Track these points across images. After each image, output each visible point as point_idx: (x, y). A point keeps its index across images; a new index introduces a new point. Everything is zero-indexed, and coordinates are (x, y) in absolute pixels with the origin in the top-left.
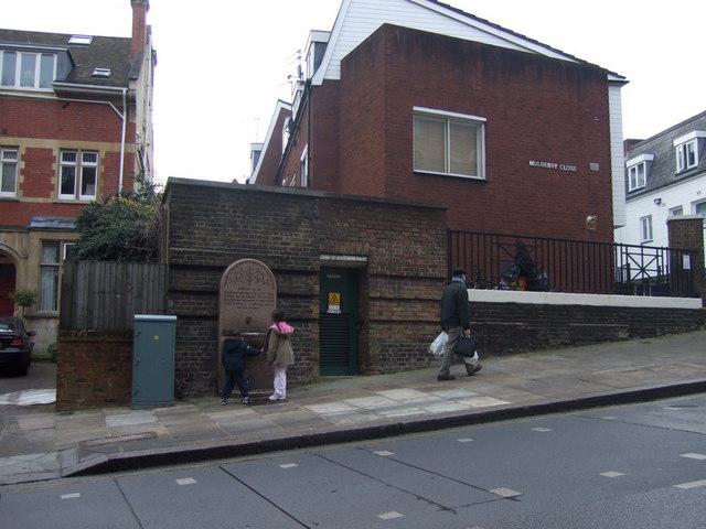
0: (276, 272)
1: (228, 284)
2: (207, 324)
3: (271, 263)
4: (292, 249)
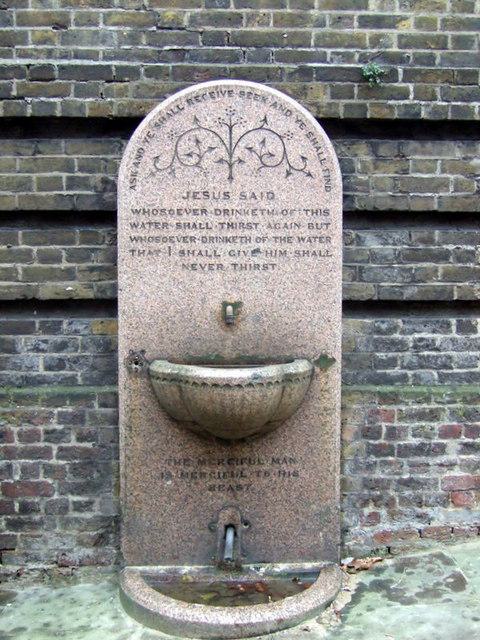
0: (337, 128)
1: (142, 180)
2: (80, 328)
3: (325, 99)
4: (406, 42)
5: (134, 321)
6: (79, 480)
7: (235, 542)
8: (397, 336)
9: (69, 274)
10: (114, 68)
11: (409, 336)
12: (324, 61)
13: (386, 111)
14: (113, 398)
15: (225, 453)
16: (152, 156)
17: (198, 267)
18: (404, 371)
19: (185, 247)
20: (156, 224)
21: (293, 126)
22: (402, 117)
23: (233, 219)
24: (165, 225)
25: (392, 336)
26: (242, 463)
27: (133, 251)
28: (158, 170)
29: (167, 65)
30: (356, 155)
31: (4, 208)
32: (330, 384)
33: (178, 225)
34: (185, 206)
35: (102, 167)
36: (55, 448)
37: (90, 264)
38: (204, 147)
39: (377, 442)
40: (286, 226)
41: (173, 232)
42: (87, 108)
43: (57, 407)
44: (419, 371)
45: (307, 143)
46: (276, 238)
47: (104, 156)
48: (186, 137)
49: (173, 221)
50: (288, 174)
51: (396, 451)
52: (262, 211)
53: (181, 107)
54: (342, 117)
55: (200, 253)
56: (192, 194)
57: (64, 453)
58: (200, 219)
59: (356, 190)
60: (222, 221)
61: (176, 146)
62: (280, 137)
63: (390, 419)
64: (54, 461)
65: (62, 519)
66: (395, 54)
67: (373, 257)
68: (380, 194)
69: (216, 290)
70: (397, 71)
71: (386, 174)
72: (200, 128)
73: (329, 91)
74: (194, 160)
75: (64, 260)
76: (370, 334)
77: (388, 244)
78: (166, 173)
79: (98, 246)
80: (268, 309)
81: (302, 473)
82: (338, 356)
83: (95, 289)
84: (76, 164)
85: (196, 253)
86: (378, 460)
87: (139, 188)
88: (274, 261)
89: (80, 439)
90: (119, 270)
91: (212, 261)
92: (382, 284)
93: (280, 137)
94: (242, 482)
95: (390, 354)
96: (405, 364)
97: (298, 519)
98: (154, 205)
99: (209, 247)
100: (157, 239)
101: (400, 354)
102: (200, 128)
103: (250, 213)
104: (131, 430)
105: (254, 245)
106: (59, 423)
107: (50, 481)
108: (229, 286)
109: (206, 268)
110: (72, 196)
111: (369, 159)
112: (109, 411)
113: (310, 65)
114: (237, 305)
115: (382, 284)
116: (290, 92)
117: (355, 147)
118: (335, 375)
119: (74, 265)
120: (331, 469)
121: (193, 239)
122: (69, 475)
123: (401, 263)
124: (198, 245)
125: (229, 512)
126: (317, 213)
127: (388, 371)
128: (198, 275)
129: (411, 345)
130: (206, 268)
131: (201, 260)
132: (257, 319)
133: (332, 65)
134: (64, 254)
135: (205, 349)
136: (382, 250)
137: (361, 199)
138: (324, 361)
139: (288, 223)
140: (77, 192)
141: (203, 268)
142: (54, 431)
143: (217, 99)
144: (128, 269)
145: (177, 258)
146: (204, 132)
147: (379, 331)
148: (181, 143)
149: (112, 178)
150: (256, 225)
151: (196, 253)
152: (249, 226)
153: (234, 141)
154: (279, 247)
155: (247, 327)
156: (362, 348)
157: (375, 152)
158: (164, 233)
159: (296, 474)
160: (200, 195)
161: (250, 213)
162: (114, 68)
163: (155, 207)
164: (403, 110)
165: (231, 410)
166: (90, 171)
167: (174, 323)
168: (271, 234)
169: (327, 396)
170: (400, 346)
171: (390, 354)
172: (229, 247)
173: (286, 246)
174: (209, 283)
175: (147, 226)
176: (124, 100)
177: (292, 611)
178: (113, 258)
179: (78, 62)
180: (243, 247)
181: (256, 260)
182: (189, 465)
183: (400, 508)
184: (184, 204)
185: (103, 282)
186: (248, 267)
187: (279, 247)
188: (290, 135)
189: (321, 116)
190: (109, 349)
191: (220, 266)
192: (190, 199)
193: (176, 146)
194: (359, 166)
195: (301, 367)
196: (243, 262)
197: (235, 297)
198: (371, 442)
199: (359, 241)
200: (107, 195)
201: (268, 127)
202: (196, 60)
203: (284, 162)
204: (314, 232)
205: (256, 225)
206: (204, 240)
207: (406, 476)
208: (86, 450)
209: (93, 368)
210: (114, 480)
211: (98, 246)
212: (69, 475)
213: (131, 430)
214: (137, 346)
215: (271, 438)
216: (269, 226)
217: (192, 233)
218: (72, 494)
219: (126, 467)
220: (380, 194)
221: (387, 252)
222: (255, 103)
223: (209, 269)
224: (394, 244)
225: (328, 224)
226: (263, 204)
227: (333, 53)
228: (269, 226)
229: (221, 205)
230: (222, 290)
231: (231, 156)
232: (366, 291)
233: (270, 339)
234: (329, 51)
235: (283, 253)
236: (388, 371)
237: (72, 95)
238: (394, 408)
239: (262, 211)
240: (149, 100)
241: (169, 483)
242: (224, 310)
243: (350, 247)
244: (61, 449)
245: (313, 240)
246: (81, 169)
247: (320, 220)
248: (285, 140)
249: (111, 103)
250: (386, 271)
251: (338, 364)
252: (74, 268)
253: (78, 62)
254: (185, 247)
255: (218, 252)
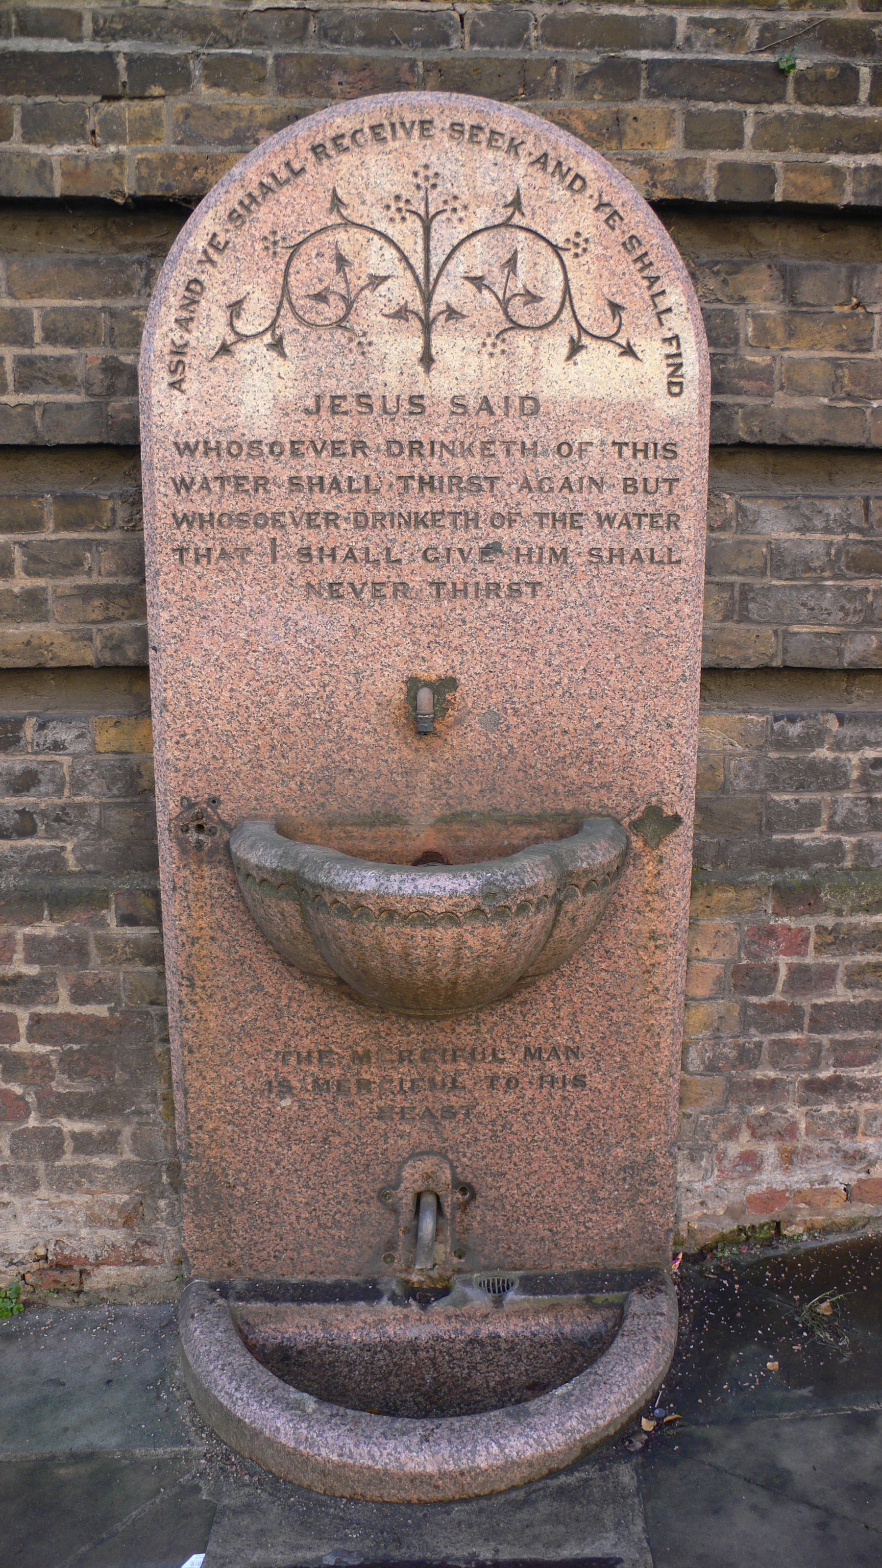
3: (670, 149)
5: (189, 726)
6: (80, 1087)
7: (438, 1230)
8: (824, 753)
9: (33, 604)
10: (122, 62)
11: (850, 755)
12: (668, 45)
13: (826, 183)
14: (149, 903)
15: (414, 1037)
16: (224, 301)
17: (345, 590)
18: (833, 836)
19: (314, 538)
20: (239, 481)
21: (588, 221)
22: (864, 201)
23: (435, 467)
24: (261, 482)
25: (812, 755)
26: (454, 1060)
27: (181, 551)
28: (242, 338)
29: (259, 52)
30: (742, 300)
31: (4, 193)
32: (666, 876)
33: (294, 483)
34: (309, 433)
35: (103, 330)
36: (23, 1016)
37: (82, 580)
38: (358, 276)
39: (765, 1000)
40: (567, 484)
41: (279, 500)
42: (57, 172)
43: (23, 924)
44: (867, 837)
45: (625, 264)
46: (541, 515)
47: (108, 302)
48: (310, 249)
49: (280, 471)
50: (575, 348)
51: (806, 1020)
52: (508, 446)
53: (297, 167)
54: (712, 199)
55: (350, 554)
56: (327, 402)
57: (40, 1028)
58: (351, 468)
59: (738, 392)
60: (404, 472)
61: (286, 274)
62: (555, 248)
63: (797, 942)
64: (22, 1046)
65: (51, 1172)
66: (853, 26)
67: (777, 560)
68: (798, 402)
69: (388, 653)
70: (857, 73)
71: (813, 352)
72: (348, 223)
73: (679, 125)
74: (333, 310)
75: (18, 570)
76: (760, 748)
77: (814, 530)
78: (259, 346)
79: (98, 536)
80: (521, 696)
81: (594, 1080)
82: (686, 809)
83: (98, 643)
84: (37, 323)
85: (341, 554)
86: (766, 1039)
87: (191, 386)
88: (537, 573)
89: (80, 996)
90: (149, 598)
91: (382, 575)
92: (795, 628)
93: (555, 248)
94: (455, 1100)
95: (806, 797)
96: (837, 819)
97: (581, 1179)
98: (231, 429)
99: (372, 540)
100: (240, 519)
101: (827, 796)
102: (348, 223)
103: (476, 450)
104: (192, 986)
105: (487, 534)
106: (29, 960)
107: (18, 1090)
108: (425, 639)
109: (366, 595)
110: (31, 407)
111: (773, 310)
112: (143, 932)
113: (631, 54)
114: (445, 686)
115: (795, 628)
116: (580, 128)
117: (741, 277)
118: (678, 851)
119: (40, 582)
120: (661, 1069)
121: (331, 519)
122: (59, 1076)
123: (842, 577)
124: (345, 535)
125: (426, 1165)
126: (645, 451)
127: (798, 837)
128: (346, 612)
129: (855, 774)
130: (366, 595)
131: (352, 573)
132: (493, 721)
133: (688, 56)
134: (18, 555)
135: (364, 794)
136: (797, 543)
137: (751, 414)
138: (658, 822)
139: (573, 478)
140: (43, 397)
141: (357, 594)
142: (18, 978)
143: (392, 145)
144: (172, 598)
145: (293, 567)
146: (360, 236)
147: (782, 742)
148: (297, 264)
149: (128, 360)
150: (492, 481)
151: (341, 554)
152: (474, 485)
153: (437, 259)
154: (546, 538)
155: (467, 740)
156: (741, 784)
157: (790, 294)
158: (258, 503)
159: (579, 1081)
160: (349, 405)
161: (476, 450)
162: (122, 62)
163: (233, 437)
164: (866, 178)
165: (429, 971)
166: (71, 341)
167: (287, 731)
168: (530, 505)
169: (659, 904)
170: (831, 777)
171: (806, 797)
172: (422, 538)
173: (565, 537)
174: (373, 632)
175: (215, 486)
176: (154, 149)
177: (572, 1431)
178: (137, 567)
179: (29, 44)
180: (460, 539)
181: (490, 572)
182: (332, 1065)
183: (810, 1143)
184: (308, 428)
185: (117, 625)
186: (471, 589)
187: (546, 538)
188: (579, 243)
189: (659, 194)
190: (134, 784)
191: (401, 589)
192: (325, 413)
193: (286, 274)
194: (749, 329)
195: (594, 853)
196: (458, 578)
197: (438, 666)
198: (754, 999)
199: (744, 520)
200: (117, 404)
201: (523, 222)
202: (335, 41)
203: (566, 314)
204: (639, 502)
205: (492, 481)
206: (360, 521)
207: (824, 1074)
208: (94, 1022)
209: (101, 831)
210: (161, 1088)
211: (98, 536)
212: (59, 1076)
213: (192, 986)
214: (199, 788)
215: (523, 1003)
216: (526, 485)
217: (329, 503)
218: (69, 1116)
219: (184, 1069)
220: (798, 402)
221: (808, 549)
222: (490, 155)
223: (374, 596)
224: (827, 530)
225: (672, 482)
226: (511, 428)
227: (692, 21)
228: (526, 485)
229: (402, 431)
230: (407, 648)
231: (427, 300)
232: (758, 645)
233: (525, 768)
234: (682, 16)
235: (560, 556)
236: (798, 837)
237: (17, 135)
238: (809, 923)
239: (508, 446)
240: (218, 150)
241: (286, 1102)
242: (412, 697)
243: (722, 536)
244: (37, 1020)
245: (634, 522)
246: (50, 337)
247: (651, 469)
248: (567, 257)
249: (118, 158)
250: (805, 597)
251: (686, 832)
252: (44, 589)
253: (29, 44)
254: (314, 538)
255: (396, 553)
